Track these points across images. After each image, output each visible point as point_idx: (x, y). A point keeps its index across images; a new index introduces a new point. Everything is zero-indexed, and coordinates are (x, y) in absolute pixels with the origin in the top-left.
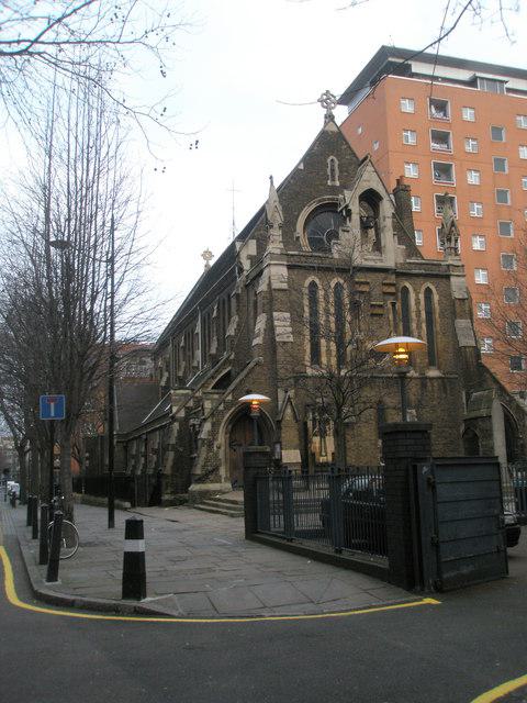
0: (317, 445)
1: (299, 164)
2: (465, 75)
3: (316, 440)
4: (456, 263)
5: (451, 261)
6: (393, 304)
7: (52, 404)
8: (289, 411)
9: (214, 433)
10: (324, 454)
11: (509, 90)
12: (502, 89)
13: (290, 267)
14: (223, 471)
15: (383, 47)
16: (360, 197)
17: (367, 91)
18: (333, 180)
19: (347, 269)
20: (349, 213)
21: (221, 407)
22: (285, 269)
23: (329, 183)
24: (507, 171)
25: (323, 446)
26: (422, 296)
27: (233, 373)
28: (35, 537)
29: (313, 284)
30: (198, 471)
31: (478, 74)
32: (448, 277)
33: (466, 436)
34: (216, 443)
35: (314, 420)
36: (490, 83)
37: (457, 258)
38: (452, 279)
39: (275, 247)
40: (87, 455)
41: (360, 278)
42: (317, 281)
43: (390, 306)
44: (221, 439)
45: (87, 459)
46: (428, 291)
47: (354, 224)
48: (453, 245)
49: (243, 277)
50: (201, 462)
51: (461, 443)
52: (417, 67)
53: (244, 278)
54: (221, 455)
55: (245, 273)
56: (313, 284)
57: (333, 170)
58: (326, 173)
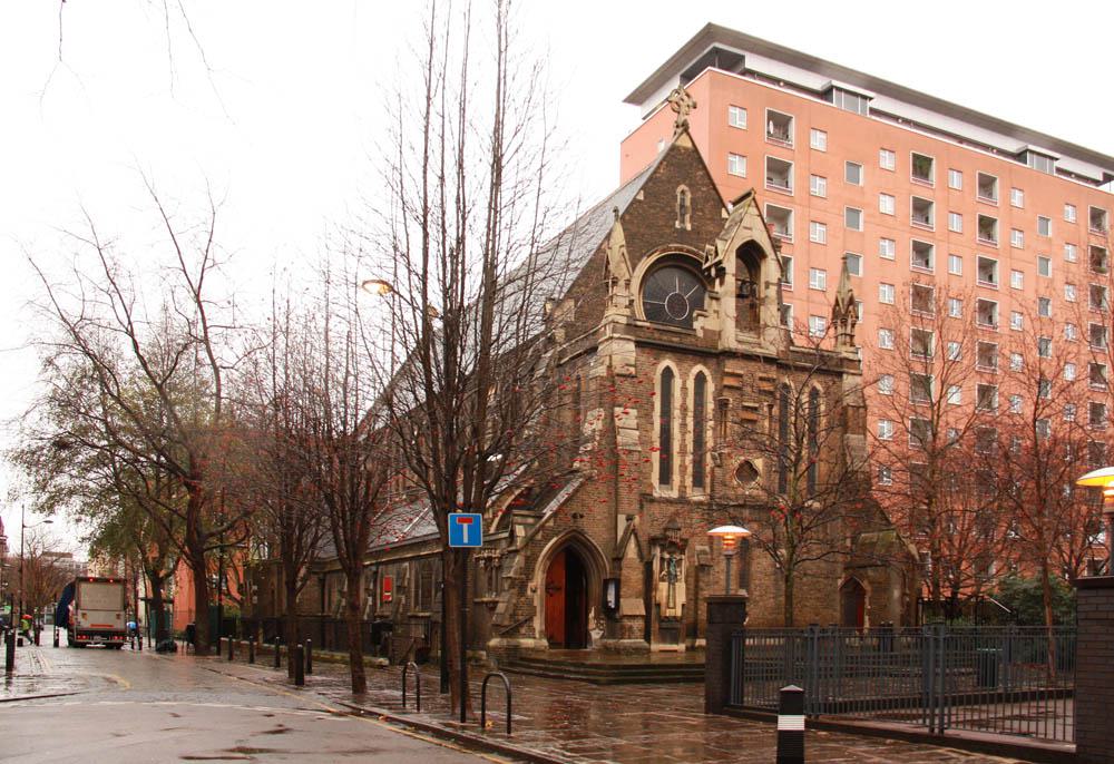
0: (665, 594)
2: (1013, 145)
3: (663, 586)
4: (851, 356)
5: (845, 351)
6: (770, 407)
7: (465, 525)
8: (632, 546)
9: (528, 570)
10: (671, 605)
11: (873, 111)
12: (864, 106)
13: (639, 344)
15: (710, 25)
17: (676, 83)
18: (683, 222)
19: (711, 353)
20: (721, 272)
21: (539, 537)
22: (632, 346)
23: (677, 225)
24: (861, 229)
25: (671, 595)
26: (691, 384)
29: (668, 371)
31: (1031, 147)
32: (840, 374)
33: (844, 590)
34: (531, 585)
35: (662, 559)
36: (848, 96)
37: (852, 349)
38: (845, 376)
40: (255, 588)
41: (731, 366)
42: (706, 372)
43: (766, 409)
45: (255, 593)
46: (700, 379)
47: (727, 288)
48: (849, 331)
51: (838, 597)
52: (752, 62)
54: (537, 603)
56: (668, 371)
58: (673, 211)
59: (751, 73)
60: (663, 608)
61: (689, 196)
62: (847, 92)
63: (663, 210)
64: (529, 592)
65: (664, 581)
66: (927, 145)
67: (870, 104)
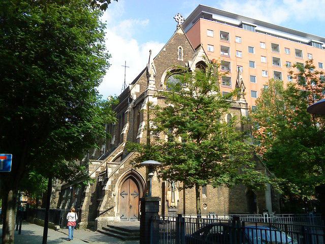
0: (170, 196)
1: (163, 48)
3: (169, 193)
5: (70, 227)
9: (112, 187)
14: (115, 209)
16: (196, 65)
21: (117, 172)
23: (178, 59)
25: (173, 196)
27: (124, 154)
28: (108, 226)
30: (102, 209)
39: (152, 86)
44: (117, 190)
49: (132, 104)
50: (103, 204)
52: (214, 17)
53: (133, 104)
54: (116, 200)
55: (133, 101)
57: (180, 53)
59: (215, 20)
60: (169, 203)
61: (182, 49)
62: (317, 43)
63: (173, 54)
64: (112, 196)
65: (170, 190)
66: (276, 41)
67: (255, 28)
